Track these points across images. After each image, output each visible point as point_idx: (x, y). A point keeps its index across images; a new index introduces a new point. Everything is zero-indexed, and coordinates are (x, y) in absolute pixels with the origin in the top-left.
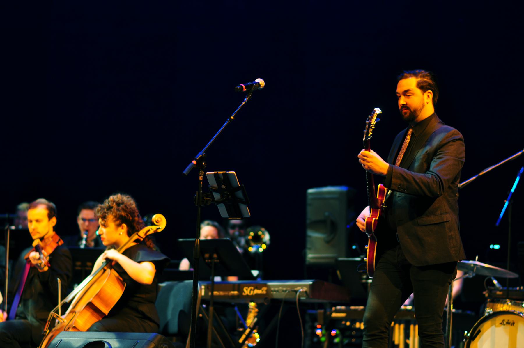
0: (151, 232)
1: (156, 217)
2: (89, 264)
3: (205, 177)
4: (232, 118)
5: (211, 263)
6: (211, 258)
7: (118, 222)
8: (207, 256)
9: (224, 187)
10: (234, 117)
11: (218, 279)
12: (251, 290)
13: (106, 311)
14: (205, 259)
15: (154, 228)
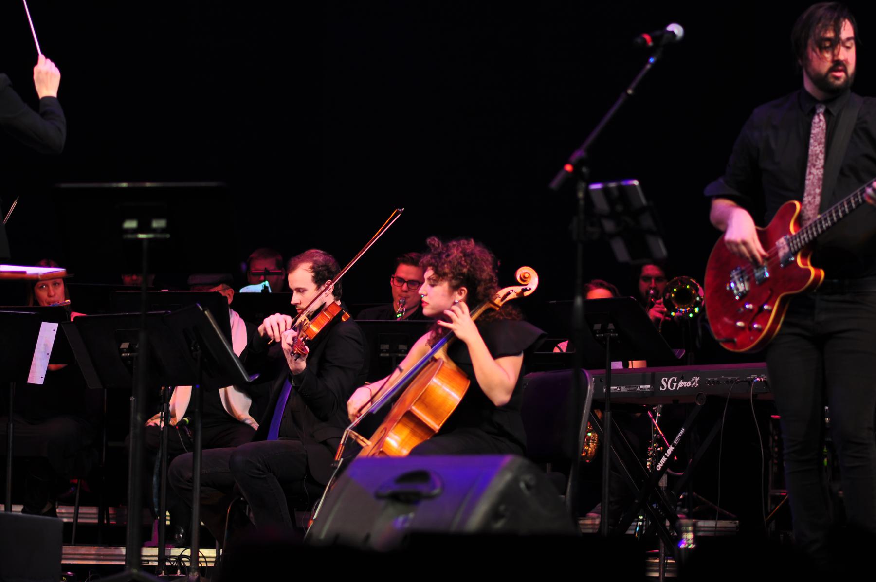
0: (513, 296)
1: (524, 271)
2: (402, 347)
3: (587, 192)
4: (630, 92)
5: (605, 338)
6: (604, 330)
7: (454, 282)
8: (597, 327)
9: (619, 208)
10: (635, 90)
11: (617, 365)
12: (673, 381)
13: (436, 426)
14: (594, 332)
15: (518, 289)
